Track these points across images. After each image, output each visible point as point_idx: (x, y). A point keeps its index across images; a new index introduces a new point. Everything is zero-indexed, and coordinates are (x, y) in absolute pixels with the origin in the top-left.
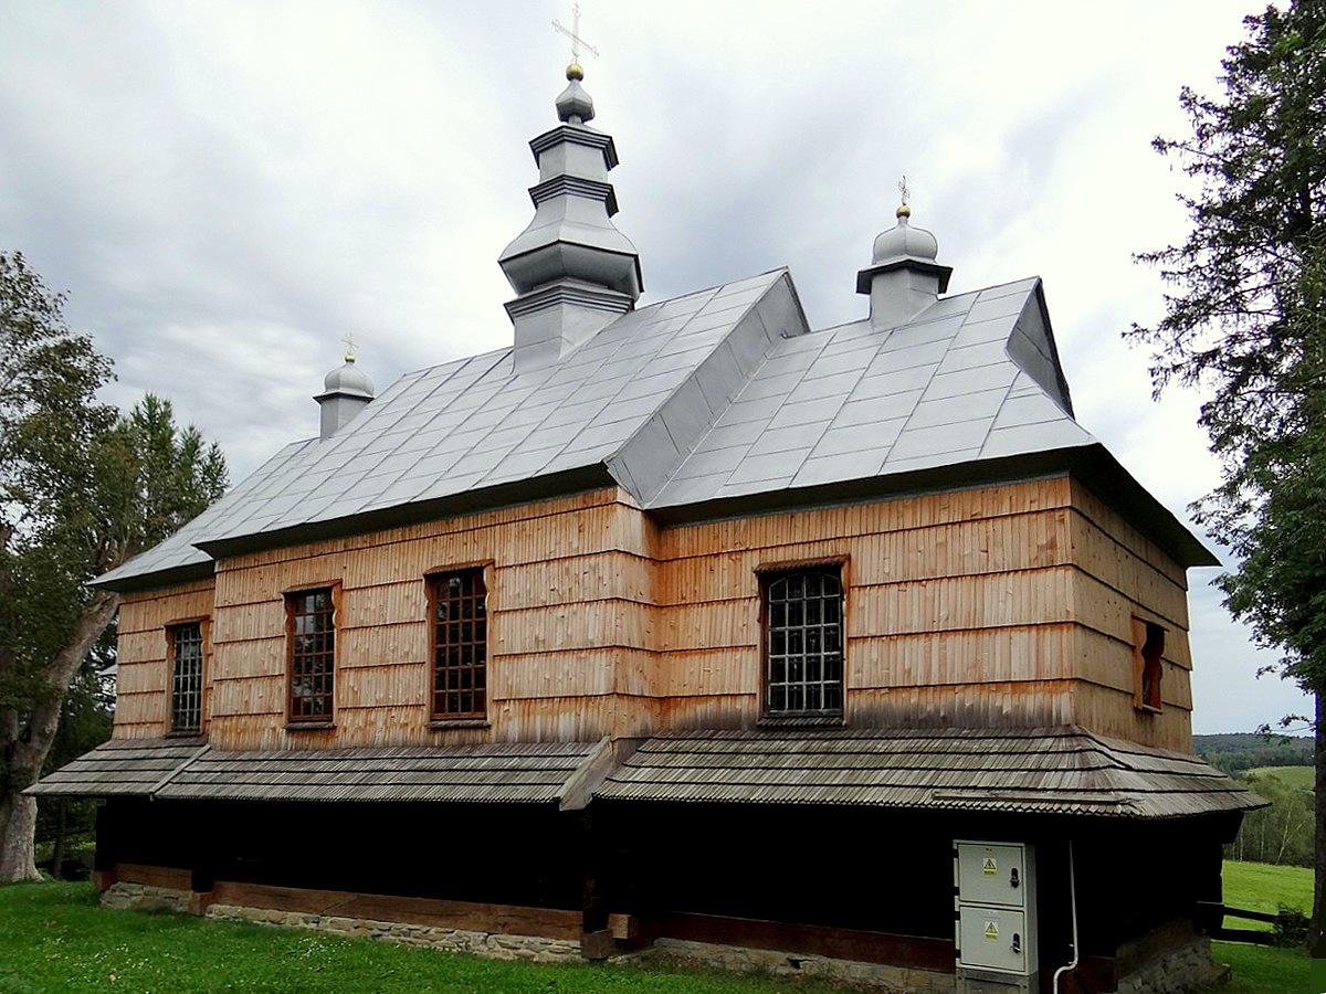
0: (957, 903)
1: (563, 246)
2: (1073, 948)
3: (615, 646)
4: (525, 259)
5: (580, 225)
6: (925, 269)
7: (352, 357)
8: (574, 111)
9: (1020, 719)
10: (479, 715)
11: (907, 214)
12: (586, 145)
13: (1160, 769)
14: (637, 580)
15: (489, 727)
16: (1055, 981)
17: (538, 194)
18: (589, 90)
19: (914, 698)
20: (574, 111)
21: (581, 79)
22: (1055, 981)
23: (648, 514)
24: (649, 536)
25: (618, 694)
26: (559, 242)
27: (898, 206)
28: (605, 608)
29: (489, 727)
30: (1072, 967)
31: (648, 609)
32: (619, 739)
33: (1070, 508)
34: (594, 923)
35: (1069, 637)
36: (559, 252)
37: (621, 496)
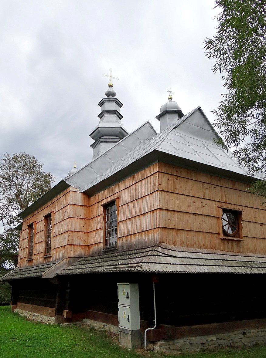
0: (119, 305)
1: (100, 128)
2: (155, 321)
3: (68, 231)
4: (94, 134)
5: (110, 122)
6: (171, 112)
7: (75, 167)
8: (110, 94)
9: (150, 242)
10: (49, 254)
11: (171, 99)
12: (118, 104)
13: (240, 266)
14: (81, 212)
15: (51, 256)
16: (145, 334)
17: (101, 116)
18: (113, 90)
19: (129, 239)
20: (110, 94)
21: (112, 87)
22: (145, 334)
23: (84, 193)
24: (85, 199)
25: (69, 245)
26: (99, 127)
27: (168, 97)
28: (168, 234)
29: (51, 256)
30: (153, 329)
31: (163, 229)
32: (69, 258)
33: (158, 172)
34: (59, 312)
35: (156, 214)
36: (99, 131)
37: (71, 189)
